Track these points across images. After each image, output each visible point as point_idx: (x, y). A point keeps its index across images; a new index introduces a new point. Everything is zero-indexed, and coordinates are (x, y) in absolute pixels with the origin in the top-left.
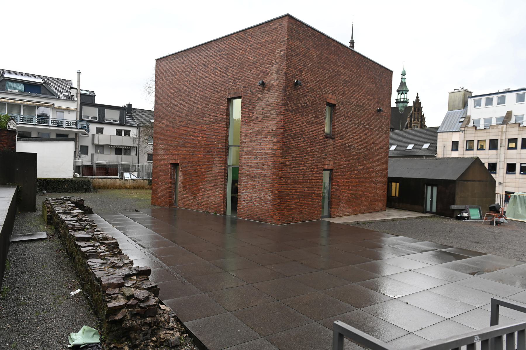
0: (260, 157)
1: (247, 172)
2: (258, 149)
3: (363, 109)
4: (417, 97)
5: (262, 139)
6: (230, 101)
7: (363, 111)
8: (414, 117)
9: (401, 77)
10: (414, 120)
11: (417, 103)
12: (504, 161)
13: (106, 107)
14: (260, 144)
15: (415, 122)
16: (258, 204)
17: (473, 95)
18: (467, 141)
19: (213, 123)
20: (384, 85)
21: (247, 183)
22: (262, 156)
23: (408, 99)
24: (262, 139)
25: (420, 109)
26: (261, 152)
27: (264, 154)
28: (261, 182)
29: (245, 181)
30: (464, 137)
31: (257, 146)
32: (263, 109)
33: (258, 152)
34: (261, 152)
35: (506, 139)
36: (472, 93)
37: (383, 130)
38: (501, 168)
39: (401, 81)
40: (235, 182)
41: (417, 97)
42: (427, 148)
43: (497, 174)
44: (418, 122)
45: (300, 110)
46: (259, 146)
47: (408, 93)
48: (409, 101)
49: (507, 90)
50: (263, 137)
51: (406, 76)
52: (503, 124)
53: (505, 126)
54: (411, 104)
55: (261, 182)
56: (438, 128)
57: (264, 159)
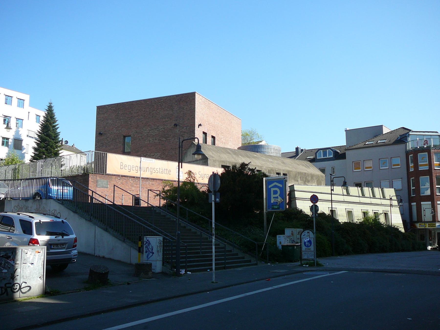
45: (104, 145)
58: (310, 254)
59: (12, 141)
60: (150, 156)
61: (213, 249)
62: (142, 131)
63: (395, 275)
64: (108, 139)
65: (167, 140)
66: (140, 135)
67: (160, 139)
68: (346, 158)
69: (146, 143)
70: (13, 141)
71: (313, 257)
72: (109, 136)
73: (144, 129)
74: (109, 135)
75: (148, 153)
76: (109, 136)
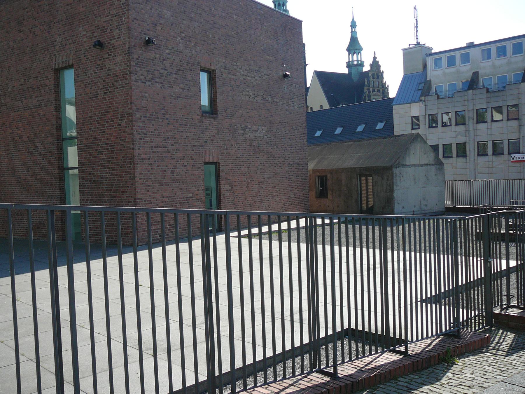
0: (105, 151)
1: (90, 174)
2: (102, 140)
3: (260, 75)
4: (375, 58)
5: (105, 125)
6: (58, 72)
7: (259, 77)
8: (373, 85)
9: (349, 29)
10: (374, 91)
11: (375, 64)
12: (474, 140)
13: (90, 297)
14: (104, 132)
15: (374, 93)
16: (108, 219)
17: (433, 51)
18: (429, 115)
19: (38, 107)
20: (290, 40)
21: (91, 190)
22: (108, 149)
23: (364, 62)
24: (105, 125)
25: (380, 74)
26: (106, 144)
27: (110, 146)
28: (110, 188)
29: (89, 188)
30: (425, 110)
31: (99, 135)
32: (104, 81)
33: (102, 145)
34: (106, 144)
35: (473, 109)
36: (431, 49)
37: (295, 103)
38: (471, 149)
39: (352, 35)
40: (111, 212)
41: (375, 58)
42: (382, 128)
43: (468, 158)
44: (379, 93)
45: (157, 80)
46: (103, 135)
47: (362, 52)
48: (365, 64)
49: (471, 45)
50: (106, 122)
51: (358, 29)
52: (469, 89)
53: (471, 91)
54: (366, 68)
55: (110, 188)
56: (393, 100)
57: (111, 153)
58: (373, 123)
59: (68, 136)
60: (251, 130)
61: (217, 371)
62: (235, 67)
63: (520, 285)
64: (165, 62)
65: (274, 102)
66: (233, 77)
67: (264, 96)
68: (405, 55)
69: (243, 99)
70: (67, 137)
71: (506, 303)
72: (169, 56)
73: (238, 64)
74: (167, 51)
75: (248, 124)
76: (169, 56)
